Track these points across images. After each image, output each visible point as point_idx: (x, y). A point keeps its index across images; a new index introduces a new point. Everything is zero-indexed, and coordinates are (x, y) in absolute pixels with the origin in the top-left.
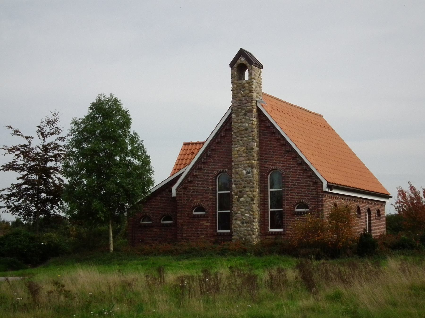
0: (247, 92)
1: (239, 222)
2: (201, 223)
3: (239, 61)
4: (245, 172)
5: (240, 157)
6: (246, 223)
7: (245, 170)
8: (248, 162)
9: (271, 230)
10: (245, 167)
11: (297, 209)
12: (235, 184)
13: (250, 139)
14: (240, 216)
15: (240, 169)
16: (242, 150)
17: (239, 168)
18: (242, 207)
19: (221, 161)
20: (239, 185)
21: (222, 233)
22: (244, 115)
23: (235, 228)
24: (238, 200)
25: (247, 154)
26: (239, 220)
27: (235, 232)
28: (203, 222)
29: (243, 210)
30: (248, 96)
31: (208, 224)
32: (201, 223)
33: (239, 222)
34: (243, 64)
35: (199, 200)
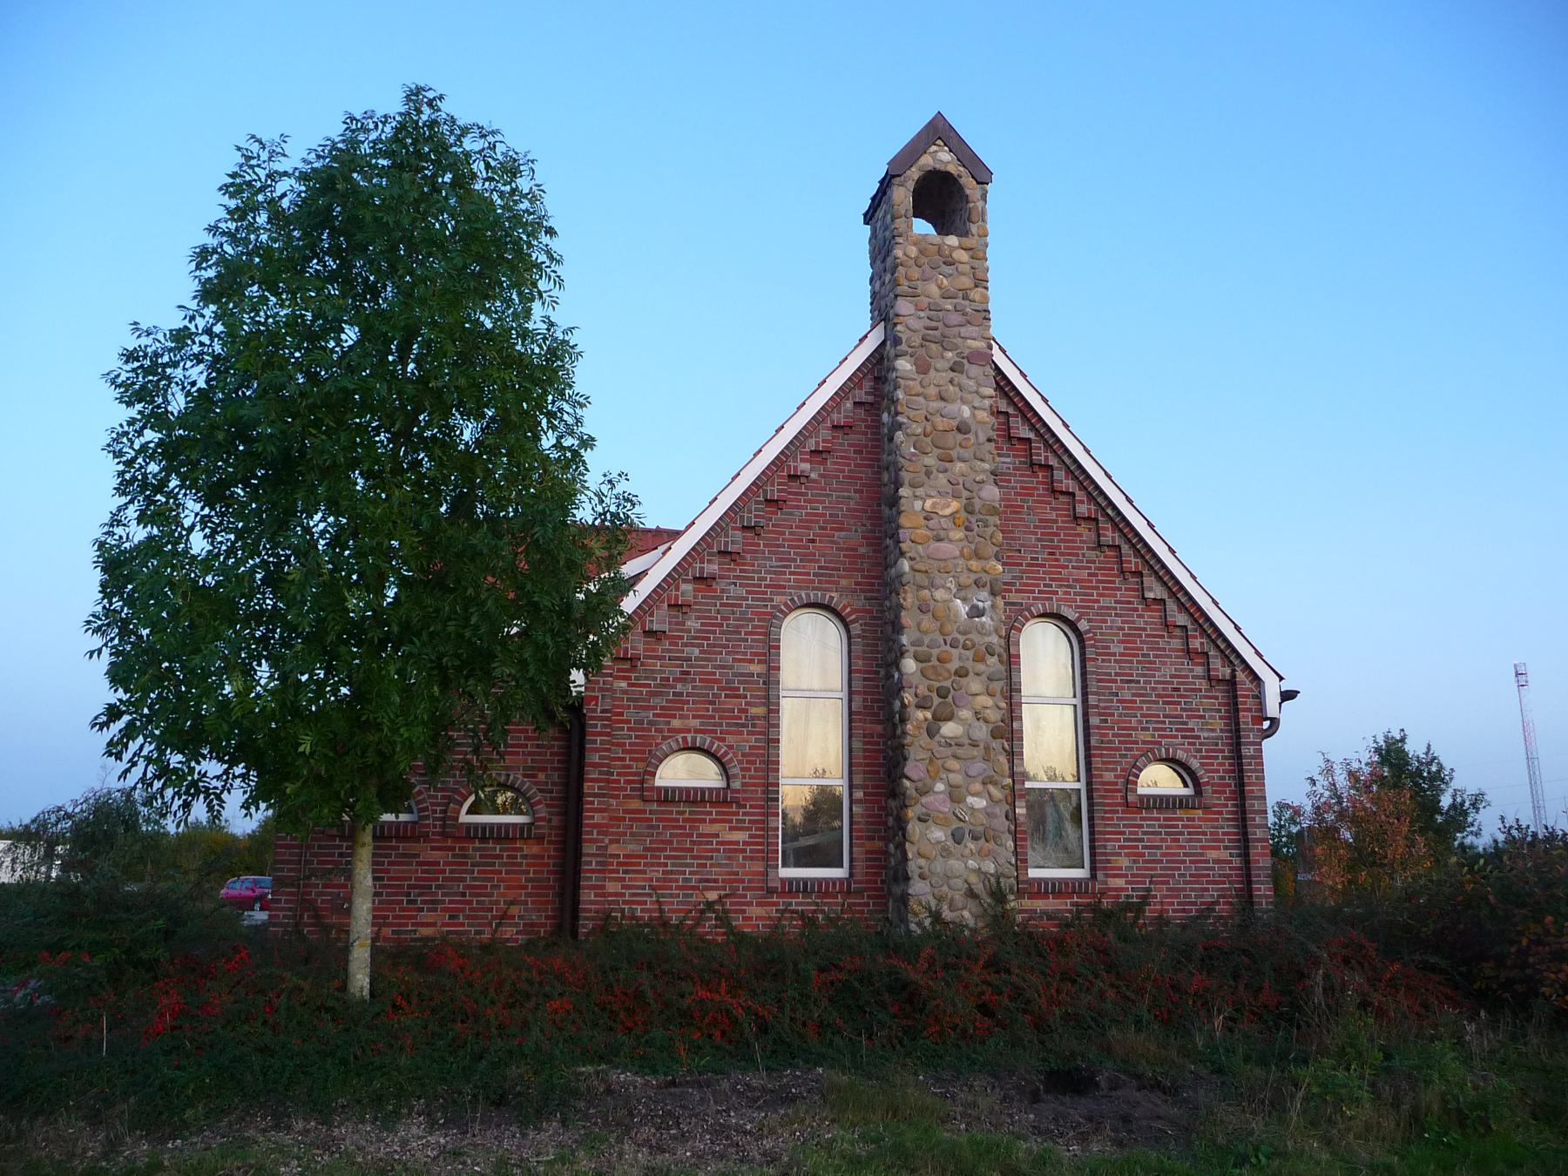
0: (967, 282)
1: (938, 834)
2: (705, 828)
3: (927, 161)
4: (962, 608)
5: (940, 540)
6: (975, 838)
7: (964, 600)
8: (974, 564)
9: (787, 873)
10: (961, 587)
11: (469, 812)
12: (917, 658)
13: (984, 471)
14: (946, 808)
15: (940, 594)
16: (948, 512)
17: (932, 586)
18: (953, 764)
19: (808, 558)
20: (934, 662)
21: (820, 881)
22: (952, 370)
23: (922, 862)
24: (932, 732)
25: (968, 529)
26: (942, 823)
27: (922, 877)
28: (716, 827)
29: (956, 778)
30: (965, 298)
31: (741, 836)
32: (705, 828)
33: (938, 834)
34: (936, 191)
35: (695, 723)
